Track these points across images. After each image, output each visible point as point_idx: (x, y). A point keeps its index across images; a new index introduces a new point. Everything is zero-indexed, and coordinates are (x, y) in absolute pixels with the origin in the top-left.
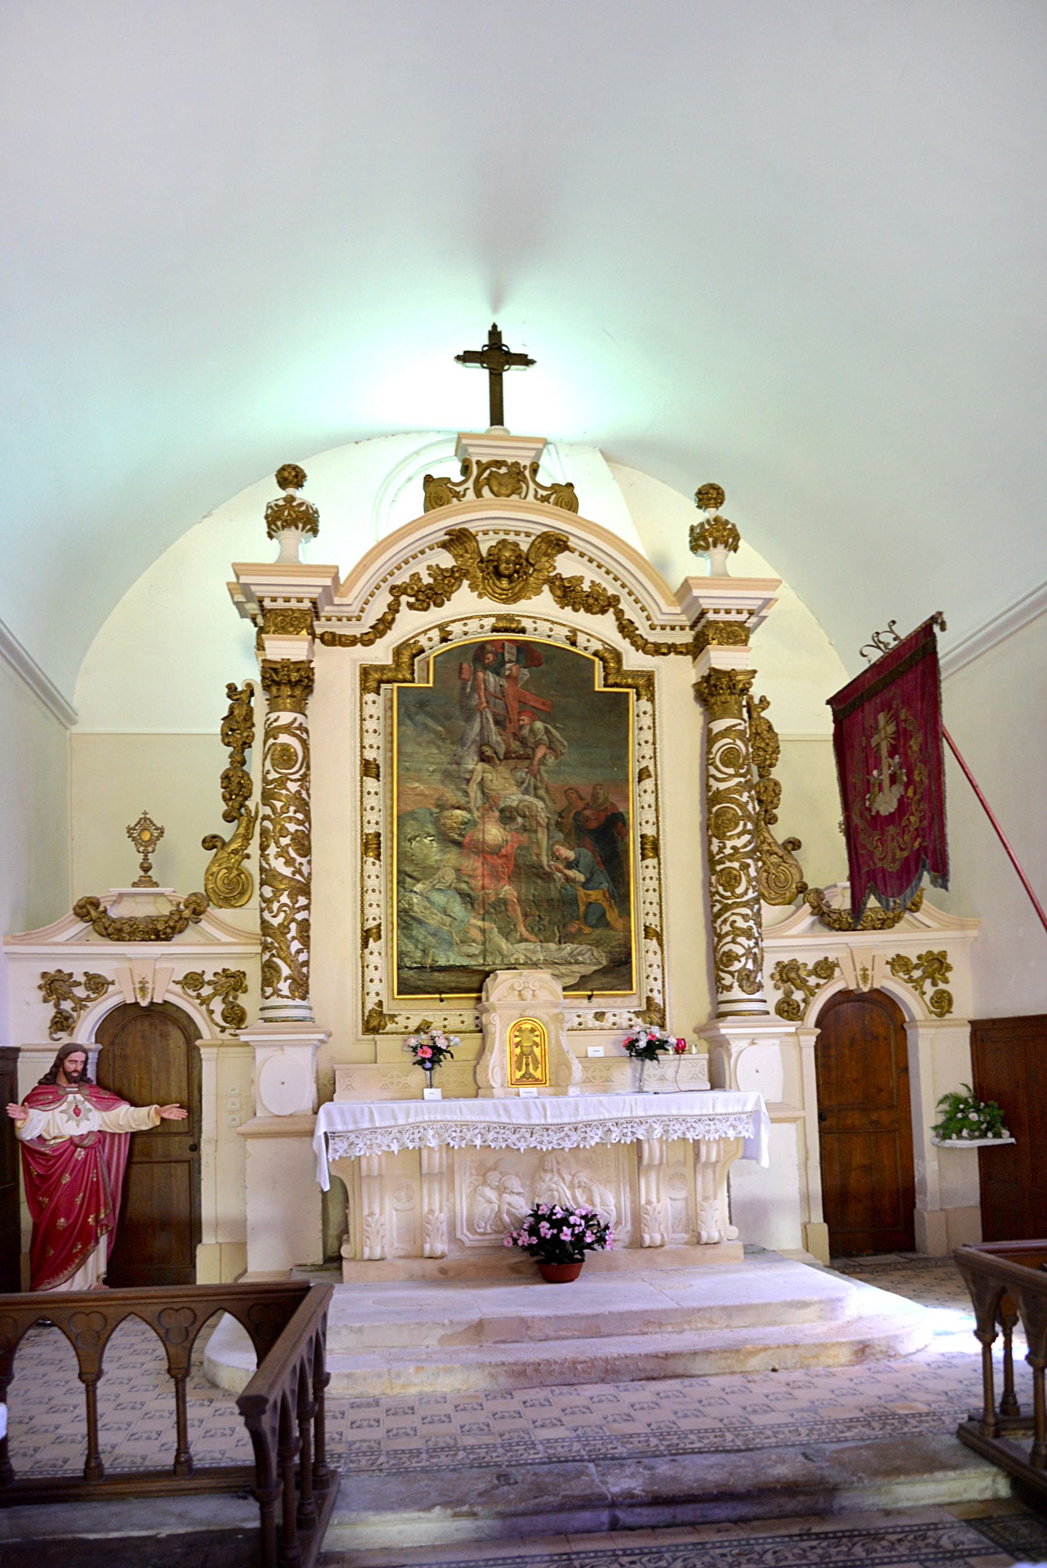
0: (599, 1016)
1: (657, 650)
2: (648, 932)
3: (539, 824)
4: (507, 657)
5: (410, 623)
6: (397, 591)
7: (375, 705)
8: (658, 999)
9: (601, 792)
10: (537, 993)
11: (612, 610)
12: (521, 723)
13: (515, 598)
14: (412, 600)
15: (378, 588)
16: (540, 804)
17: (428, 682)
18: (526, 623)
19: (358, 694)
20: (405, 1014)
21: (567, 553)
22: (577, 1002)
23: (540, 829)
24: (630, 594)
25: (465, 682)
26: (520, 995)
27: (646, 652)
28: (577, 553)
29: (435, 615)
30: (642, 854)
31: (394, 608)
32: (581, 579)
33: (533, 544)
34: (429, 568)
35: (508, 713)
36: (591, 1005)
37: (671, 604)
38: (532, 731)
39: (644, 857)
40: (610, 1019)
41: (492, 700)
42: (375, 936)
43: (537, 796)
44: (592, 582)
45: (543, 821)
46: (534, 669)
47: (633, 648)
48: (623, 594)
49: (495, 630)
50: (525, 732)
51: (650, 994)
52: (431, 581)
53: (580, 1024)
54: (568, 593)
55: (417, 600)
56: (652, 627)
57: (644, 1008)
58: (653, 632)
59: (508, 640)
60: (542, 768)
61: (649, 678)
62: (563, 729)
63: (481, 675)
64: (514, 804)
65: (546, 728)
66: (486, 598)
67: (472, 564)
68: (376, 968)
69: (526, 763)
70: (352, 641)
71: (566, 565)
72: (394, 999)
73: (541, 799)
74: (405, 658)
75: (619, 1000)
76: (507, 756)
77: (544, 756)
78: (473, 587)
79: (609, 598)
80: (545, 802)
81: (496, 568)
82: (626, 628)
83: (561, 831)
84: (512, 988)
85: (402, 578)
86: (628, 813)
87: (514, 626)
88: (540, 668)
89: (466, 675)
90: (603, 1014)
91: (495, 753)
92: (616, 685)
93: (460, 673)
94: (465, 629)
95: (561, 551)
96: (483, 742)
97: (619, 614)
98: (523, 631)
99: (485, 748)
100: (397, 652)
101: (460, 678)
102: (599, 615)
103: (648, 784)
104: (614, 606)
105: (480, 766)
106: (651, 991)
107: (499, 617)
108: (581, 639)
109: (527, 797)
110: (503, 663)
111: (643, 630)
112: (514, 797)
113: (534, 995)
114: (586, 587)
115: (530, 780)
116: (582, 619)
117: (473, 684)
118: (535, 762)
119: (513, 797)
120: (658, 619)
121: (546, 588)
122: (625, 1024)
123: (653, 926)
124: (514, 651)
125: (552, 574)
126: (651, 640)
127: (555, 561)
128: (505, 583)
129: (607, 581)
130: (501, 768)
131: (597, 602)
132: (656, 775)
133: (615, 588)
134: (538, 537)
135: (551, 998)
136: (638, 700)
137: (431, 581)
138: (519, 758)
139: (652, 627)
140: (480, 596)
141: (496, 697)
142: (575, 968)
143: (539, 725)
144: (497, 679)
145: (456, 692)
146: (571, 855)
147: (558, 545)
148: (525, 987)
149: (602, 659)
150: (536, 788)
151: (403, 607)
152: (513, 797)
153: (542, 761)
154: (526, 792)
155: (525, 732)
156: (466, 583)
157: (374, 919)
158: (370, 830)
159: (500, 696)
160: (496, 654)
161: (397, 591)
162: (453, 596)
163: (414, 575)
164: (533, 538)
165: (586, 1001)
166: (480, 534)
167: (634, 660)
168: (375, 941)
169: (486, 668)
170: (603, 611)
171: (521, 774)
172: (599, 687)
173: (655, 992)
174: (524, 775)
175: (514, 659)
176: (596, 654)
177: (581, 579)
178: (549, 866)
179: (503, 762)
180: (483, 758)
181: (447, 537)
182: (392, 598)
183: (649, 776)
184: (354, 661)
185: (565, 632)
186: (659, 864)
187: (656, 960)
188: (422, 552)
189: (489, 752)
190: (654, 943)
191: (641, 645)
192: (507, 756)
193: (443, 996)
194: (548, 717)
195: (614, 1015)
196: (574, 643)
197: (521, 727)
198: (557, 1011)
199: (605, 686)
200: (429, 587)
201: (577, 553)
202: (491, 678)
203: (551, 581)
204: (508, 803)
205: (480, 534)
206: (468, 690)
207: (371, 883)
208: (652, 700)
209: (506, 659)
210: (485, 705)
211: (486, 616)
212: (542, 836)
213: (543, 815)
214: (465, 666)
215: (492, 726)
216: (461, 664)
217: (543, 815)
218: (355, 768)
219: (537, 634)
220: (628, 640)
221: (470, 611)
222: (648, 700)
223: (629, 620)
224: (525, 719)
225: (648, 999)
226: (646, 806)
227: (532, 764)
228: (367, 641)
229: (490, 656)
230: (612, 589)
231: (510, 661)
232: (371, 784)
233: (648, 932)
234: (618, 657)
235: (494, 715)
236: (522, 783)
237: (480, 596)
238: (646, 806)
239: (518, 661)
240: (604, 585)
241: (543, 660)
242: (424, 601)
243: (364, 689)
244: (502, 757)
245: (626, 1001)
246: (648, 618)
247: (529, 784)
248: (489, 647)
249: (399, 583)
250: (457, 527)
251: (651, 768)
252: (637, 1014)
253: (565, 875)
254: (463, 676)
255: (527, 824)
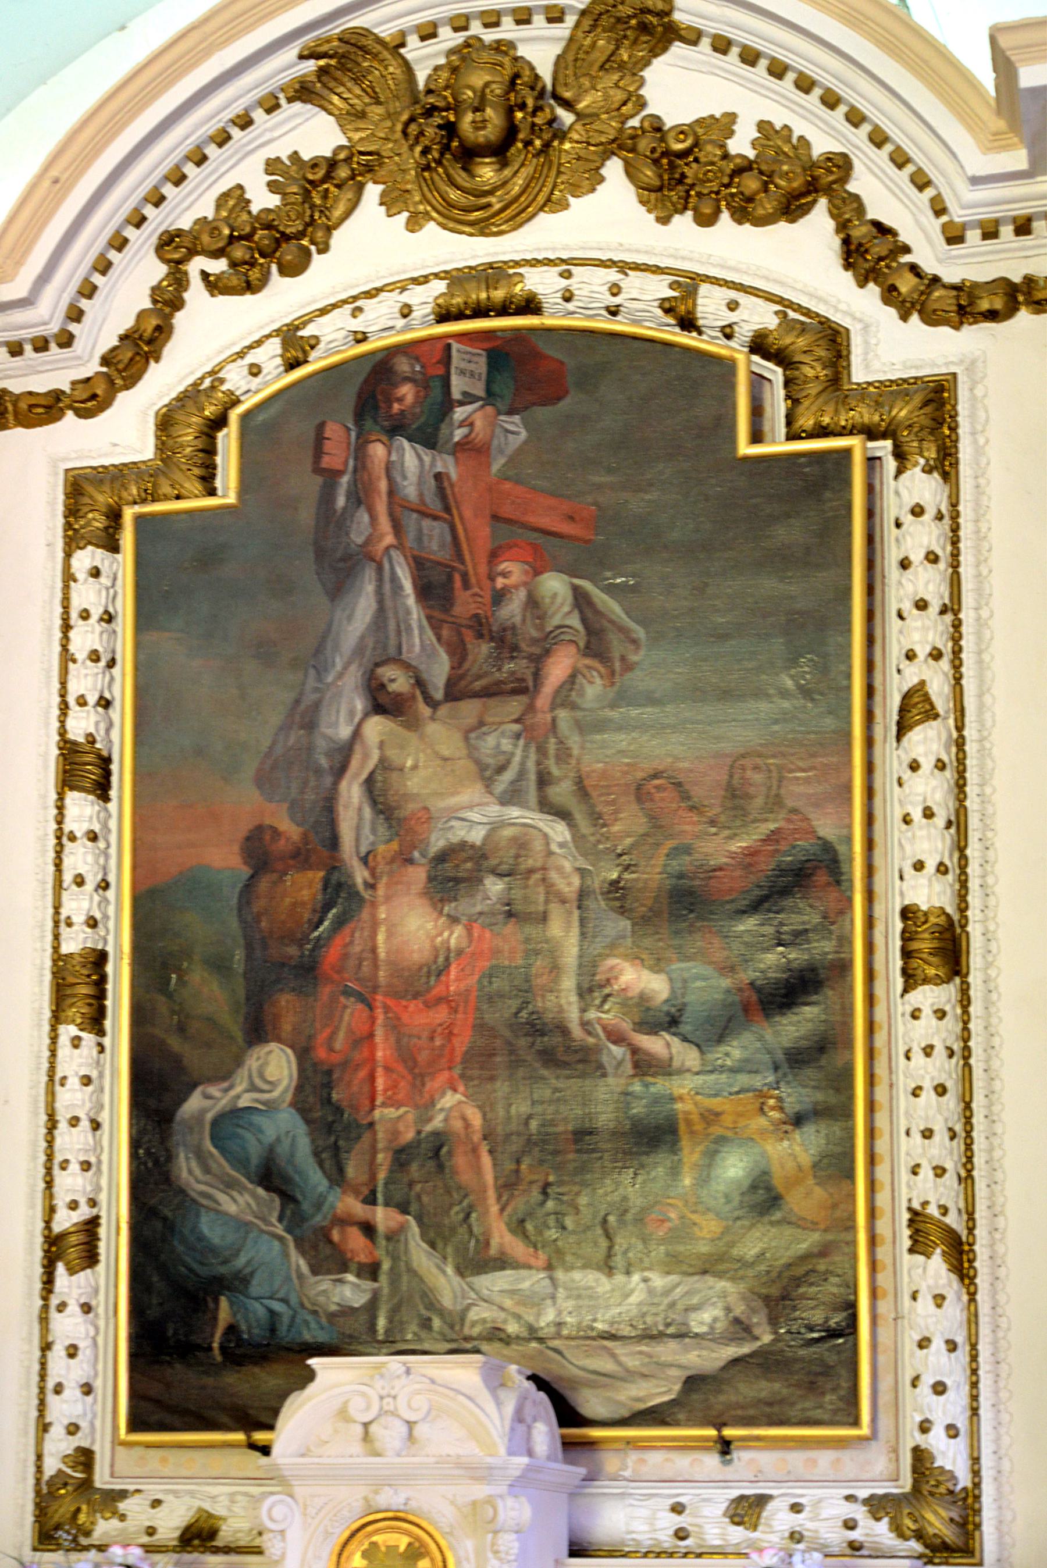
0: (747, 1510)
1: (965, 306)
2: (922, 1231)
3: (552, 893)
4: (458, 385)
5: (221, 336)
6: (175, 248)
7: (110, 580)
8: (950, 1456)
9: (758, 778)
10: (419, 1430)
11: (823, 202)
12: (500, 582)
13: (517, 214)
14: (218, 266)
15: (120, 243)
16: (559, 831)
17: (208, 484)
18: (542, 283)
19: (60, 555)
20: (154, 1489)
21: (678, 49)
22: (682, 1462)
23: (556, 912)
24: (878, 139)
25: (332, 476)
26: (367, 1437)
27: (931, 319)
28: (705, 43)
29: (283, 298)
30: (904, 972)
31: (168, 300)
32: (726, 124)
33: (571, 40)
34: (272, 165)
35: (459, 556)
36: (729, 1472)
37: (995, 144)
38: (533, 603)
39: (911, 980)
40: (778, 1519)
41: (411, 520)
42: (73, 1253)
43: (546, 806)
44: (764, 126)
45: (569, 885)
46: (542, 413)
47: (892, 312)
48: (853, 141)
49: (443, 316)
50: (513, 609)
51: (919, 1439)
52: (274, 201)
53: (681, 1534)
54: (682, 174)
55: (233, 264)
56: (954, 237)
57: (906, 1484)
58: (957, 250)
59: (461, 336)
60: (562, 714)
61: (937, 398)
62: (634, 589)
63: (378, 451)
64: (476, 836)
65: (576, 590)
66: (431, 228)
67: (378, 132)
68: (72, 1352)
69: (515, 705)
70: (46, 409)
71: (678, 89)
72: (874, 1436)
73: (563, 814)
74: (188, 437)
75: (825, 1458)
76: (455, 692)
77: (572, 678)
78: (390, 203)
79: (814, 165)
80: (572, 824)
81: (450, 129)
82: (870, 252)
83: (622, 911)
84: (343, 1414)
85: (193, 206)
86: (849, 840)
87: (499, 295)
88: (564, 405)
89: (335, 455)
90: (762, 1501)
91: (420, 683)
92: (822, 432)
93: (318, 451)
94: (357, 324)
95: (659, 48)
96: (383, 649)
97: (848, 212)
98: (531, 305)
99: (388, 672)
100: (165, 423)
101: (318, 470)
102: (782, 226)
103: (927, 741)
104: (828, 191)
105: (376, 727)
106: (925, 1427)
107: (456, 278)
108: (710, 305)
109: (514, 812)
110: (447, 405)
111: (928, 251)
112: (473, 817)
113: (410, 1436)
114: (742, 144)
115: (521, 756)
116: (725, 246)
117: (355, 482)
118: (543, 700)
119: (474, 816)
120: (967, 204)
121: (614, 168)
122: (836, 1537)
123: (933, 1210)
124: (481, 365)
125: (635, 122)
126: (951, 275)
127: (642, 83)
128: (487, 172)
129: (807, 115)
130: (433, 729)
131: (787, 184)
132: (960, 712)
133: (832, 131)
134: (583, 13)
135: (471, 1450)
136: (899, 472)
137: (274, 201)
138: (489, 693)
139: (954, 237)
140: (414, 224)
141: (424, 514)
142: (667, 1351)
143: (555, 586)
144: (427, 456)
145: (306, 515)
146: (656, 986)
147: (644, 28)
148: (382, 1413)
149: (780, 358)
150: (544, 780)
151: (196, 293)
152: (474, 816)
153: (565, 696)
154: (512, 797)
155: (513, 609)
156: (373, 191)
157: (73, 1205)
158: (73, 943)
159: (434, 505)
160: (423, 383)
161: (175, 248)
162: (338, 238)
163: (225, 196)
164: (571, 20)
165: (712, 1460)
166: (413, 40)
167: (890, 347)
168: (72, 1271)
169: (396, 428)
170: (792, 208)
171: (498, 741)
172: (745, 449)
173: (938, 1433)
174: (506, 745)
175: (479, 390)
176: (759, 346)
177: (726, 124)
178: (585, 1024)
179: (443, 710)
180: (382, 703)
181: (311, 66)
182: (162, 269)
183: (931, 714)
184: (54, 463)
185: (661, 288)
186: (965, 1001)
187: (949, 1320)
188: (245, 122)
189: (398, 682)
190: (935, 1270)
191: (928, 301)
192: (455, 692)
193: (728, 1432)
194: (585, 558)
195: (796, 1508)
196: (688, 323)
197: (499, 597)
198: (481, 1491)
199: (791, 437)
200: (267, 221)
201: (705, 43)
202: (410, 457)
203: (621, 145)
204: (459, 833)
205: (413, 40)
206: (341, 501)
207: (72, 1098)
208: (945, 465)
209: (456, 395)
210: (389, 539)
211: (417, 281)
212: (563, 933)
213: (568, 866)
214: (332, 430)
215: (411, 601)
216: (321, 427)
217: (568, 866)
218: (46, 767)
219: (574, 302)
220: (873, 289)
221: (384, 267)
222: (928, 470)
223: (878, 225)
224: (513, 571)
225: (920, 1456)
226: (917, 814)
227: (531, 708)
228: (91, 399)
229: (407, 391)
230: (823, 136)
231: (468, 398)
232: (81, 808)
233: (922, 1231)
234: (834, 340)
235: (419, 565)
236: (501, 769)
237: (414, 224)
238: (917, 814)
239: (490, 396)
240: (800, 128)
241: (570, 380)
242: (252, 264)
243: (73, 542)
244: (439, 695)
245: (849, 1461)
246: (939, 209)
247: (522, 774)
248: (403, 365)
249: (185, 223)
250: (337, 28)
251: (939, 690)
252: (876, 1506)
253: (635, 1051)
254: (326, 462)
255: (517, 894)
